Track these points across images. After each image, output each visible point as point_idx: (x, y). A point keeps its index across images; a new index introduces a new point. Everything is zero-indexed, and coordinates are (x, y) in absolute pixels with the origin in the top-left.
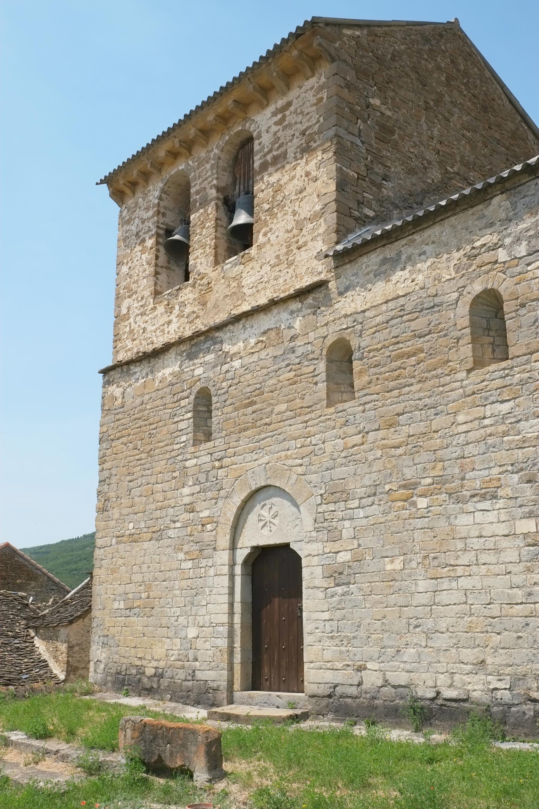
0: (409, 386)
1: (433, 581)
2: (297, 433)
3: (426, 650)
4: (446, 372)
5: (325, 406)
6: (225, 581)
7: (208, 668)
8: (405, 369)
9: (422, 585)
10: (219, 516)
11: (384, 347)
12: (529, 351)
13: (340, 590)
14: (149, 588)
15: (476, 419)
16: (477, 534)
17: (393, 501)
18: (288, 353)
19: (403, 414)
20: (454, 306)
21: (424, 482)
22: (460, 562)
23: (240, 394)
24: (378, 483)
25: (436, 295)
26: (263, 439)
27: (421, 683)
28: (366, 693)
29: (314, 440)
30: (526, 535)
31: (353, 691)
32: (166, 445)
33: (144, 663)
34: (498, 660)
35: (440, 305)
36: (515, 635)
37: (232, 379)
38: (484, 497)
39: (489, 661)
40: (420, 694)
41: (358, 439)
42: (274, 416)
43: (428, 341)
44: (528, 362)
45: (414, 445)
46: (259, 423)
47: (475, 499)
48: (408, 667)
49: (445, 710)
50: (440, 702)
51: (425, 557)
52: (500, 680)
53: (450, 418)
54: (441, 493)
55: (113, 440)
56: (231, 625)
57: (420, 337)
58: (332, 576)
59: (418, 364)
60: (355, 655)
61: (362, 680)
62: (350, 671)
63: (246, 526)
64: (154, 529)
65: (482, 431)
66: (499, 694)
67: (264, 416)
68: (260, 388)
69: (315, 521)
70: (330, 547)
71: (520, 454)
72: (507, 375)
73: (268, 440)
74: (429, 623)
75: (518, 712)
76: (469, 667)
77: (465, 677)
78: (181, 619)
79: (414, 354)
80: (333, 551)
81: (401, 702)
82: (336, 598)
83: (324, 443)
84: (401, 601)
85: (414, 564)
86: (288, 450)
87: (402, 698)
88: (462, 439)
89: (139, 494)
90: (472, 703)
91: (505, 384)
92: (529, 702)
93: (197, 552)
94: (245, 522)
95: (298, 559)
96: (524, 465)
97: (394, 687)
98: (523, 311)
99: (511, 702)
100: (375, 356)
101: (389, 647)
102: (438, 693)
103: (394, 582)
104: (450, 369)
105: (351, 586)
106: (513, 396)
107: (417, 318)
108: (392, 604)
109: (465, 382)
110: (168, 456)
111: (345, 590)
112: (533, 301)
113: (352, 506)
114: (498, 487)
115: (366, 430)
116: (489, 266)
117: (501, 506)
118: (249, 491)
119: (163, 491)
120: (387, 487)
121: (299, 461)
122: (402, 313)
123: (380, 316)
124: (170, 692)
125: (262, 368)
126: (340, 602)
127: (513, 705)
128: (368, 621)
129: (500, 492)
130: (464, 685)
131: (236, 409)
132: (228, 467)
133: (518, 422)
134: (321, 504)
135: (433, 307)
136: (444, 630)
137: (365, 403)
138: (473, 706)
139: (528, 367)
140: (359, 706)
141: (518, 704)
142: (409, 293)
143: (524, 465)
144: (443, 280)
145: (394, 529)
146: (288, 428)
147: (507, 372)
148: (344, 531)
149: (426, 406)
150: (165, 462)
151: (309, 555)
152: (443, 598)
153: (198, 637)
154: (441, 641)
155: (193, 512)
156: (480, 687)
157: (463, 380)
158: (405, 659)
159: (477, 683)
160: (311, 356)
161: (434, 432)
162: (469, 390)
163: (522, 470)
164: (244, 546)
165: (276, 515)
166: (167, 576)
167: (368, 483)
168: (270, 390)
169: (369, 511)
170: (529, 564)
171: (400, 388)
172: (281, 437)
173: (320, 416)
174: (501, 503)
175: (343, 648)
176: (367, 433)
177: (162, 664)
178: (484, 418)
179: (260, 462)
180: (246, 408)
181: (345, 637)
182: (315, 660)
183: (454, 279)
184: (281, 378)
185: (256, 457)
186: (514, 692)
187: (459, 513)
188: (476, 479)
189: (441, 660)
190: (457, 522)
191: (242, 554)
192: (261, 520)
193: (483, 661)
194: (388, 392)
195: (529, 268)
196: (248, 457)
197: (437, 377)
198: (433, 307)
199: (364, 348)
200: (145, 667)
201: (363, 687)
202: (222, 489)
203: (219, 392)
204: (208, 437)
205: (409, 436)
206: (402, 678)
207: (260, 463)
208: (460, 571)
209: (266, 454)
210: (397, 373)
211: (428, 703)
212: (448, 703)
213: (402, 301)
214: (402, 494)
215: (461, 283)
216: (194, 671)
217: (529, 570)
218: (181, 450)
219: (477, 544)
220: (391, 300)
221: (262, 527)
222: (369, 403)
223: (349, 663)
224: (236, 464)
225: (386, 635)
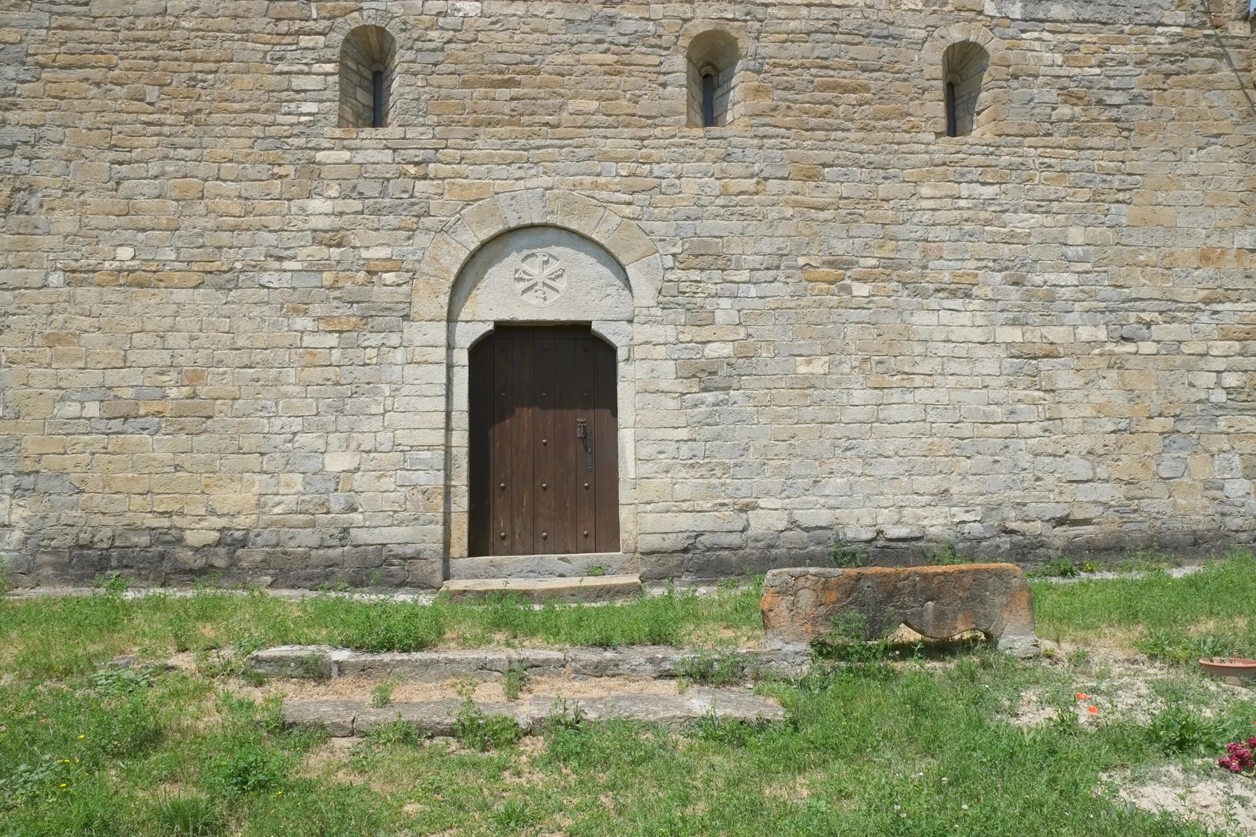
0: (843, 130)
1: (877, 391)
2: (621, 153)
3: (862, 479)
4: (904, 127)
5: (684, 122)
6: (440, 374)
7: (389, 521)
8: (837, 106)
9: (859, 396)
10: (419, 261)
11: (802, 66)
12: (1022, 132)
13: (710, 397)
14: (195, 377)
15: (947, 196)
16: (943, 337)
17: (810, 281)
18: (599, 23)
19: (831, 166)
20: (919, 47)
21: (862, 261)
22: (918, 369)
23: (478, 60)
24: (785, 252)
25: (892, 23)
26: (538, 148)
27: (854, 522)
28: (757, 541)
29: (657, 170)
30: (1009, 345)
31: (735, 539)
32: (249, 111)
33: (178, 521)
34: (967, 488)
35: (900, 38)
36: (991, 459)
37: (455, 30)
38: (953, 294)
39: (955, 489)
40: (850, 535)
41: (749, 184)
42: (565, 114)
43: (877, 80)
44: (1020, 145)
45: (851, 212)
46: (525, 119)
47: (940, 295)
48: (832, 502)
50: (881, 543)
51: (865, 360)
52: (968, 512)
53: (910, 188)
54: (890, 281)
55: (43, 66)
56: (448, 447)
57: (864, 71)
58: (694, 376)
59: (861, 105)
60: (738, 489)
62: (726, 512)
63: (481, 285)
64: (208, 267)
65: (957, 213)
66: (966, 528)
67: (541, 110)
68: (533, 63)
69: (659, 292)
70: (689, 334)
71: (1005, 250)
72: (992, 154)
73: (550, 150)
74: (870, 445)
75: (991, 546)
76: (926, 498)
77: (920, 511)
78: (301, 439)
79: (854, 91)
80: (699, 339)
81: (819, 548)
82: (703, 409)
83: (679, 177)
84: (823, 415)
85: (846, 368)
86: (599, 175)
87: (818, 544)
88: (926, 217)
89: (157, 192)
90: (930, 541)
91: (989, 163)
93: (354, 319)
94: (480, 278)
95: (611, 350)
96: (1011, 264)
97: (807, 529)
98: (1014, 84)
100: (784, 75)
101: (800, 477)
103: (811, 391)
104: (911, 124)
105: (732, 392)
106: (999, 180)
107: (861, 43)
108: (808, 419)
109: (932, 147)
110: (255, 131)
111: (721, 397)
112: (1029, 76)
113: (735, 279)
114: (974, 285)
115: (763, 174)
116: (972, 14)
117: (976, 307)
118: (501, 227)
119: (239, 197)
120: (801, 261)
121: (627, 198)
122: (834, 29)
123: (797, 22)
124: (272, 572)
125: (535, 30)
126: (710, 415)
127: (985, 539)
128: (765, 442)
129: (975, 291)
131: (465, 84)
132: (444, 179)
133: (1004, 212)
134: (672, 268)
135: (886, 37)
136: (891, 453)
137: (765, 137)
139: (1020, 151)
140: (743, 560)
142: (848, 6)
143: (1011, 264)
144: (903, 7)
145: (812, 319)
146: (601, 141)
147: (991, 149)
148: (718, 313)
149: (870, 163)
150: (249, 142)
151: (647, 343)
152: (893, 413)
153: (358, 469)
154: (884, 468)
155: (339, 245)
156: (942, 521)
157: (929, 144)
158: (827, 492)
159: (937, 517)
160: (653, 41)
161: (882, 200)
162: (938, 157)
163: (1007, 269)
164: (476, 318)
165: (561, 276)
166: (258, 358)
167: (767, 250)
168: (558, 71)
169: (767, 289)
170: (1011, 378)
171: (827, 130)
172: (583, 152)
173: (673, 136)
174: (976, 304)
175: (713, 481)
176: (766, 179)
177: (243, 521)
178: (959, 198)
179: (531, 183)
180: (494, 87)
181: (718, 464)
182: (656, 499)
183: (920, 11)
184: (583, 58)
185: (520, 173)
187: (917, 309)
188: (944, 271)
189: (886, 491)
190: (913, 320)
191: (468, 334)
192: (521, 279)
193: (946, 491)
194: (807, 130)
195: (1024, 36)
196: (501, 171)
197: (891, 129)
198: (886, 37)
199: (764, 58)
200: (182, 530)
201: (749, 533)
202: (427, 214)
203: (419, 45)
204: (376, 117)
205: (841, 198)
206: (823, 517)
207: (529, 185)
208: (918, 380)
209: (545, 173)
210: (824, 108)
212: (893, 544)
213: (836, 13)
214: (828, 274)
215: (932, 20)
216: (345, 530)
217: (1011, 385)
218: (301, 128)
219: (944, 349)
220: (815, 5)
221: (524, 292)
222: (771, 137)
223: (726, 501)
224: (467, 177)
225: (797, 461)
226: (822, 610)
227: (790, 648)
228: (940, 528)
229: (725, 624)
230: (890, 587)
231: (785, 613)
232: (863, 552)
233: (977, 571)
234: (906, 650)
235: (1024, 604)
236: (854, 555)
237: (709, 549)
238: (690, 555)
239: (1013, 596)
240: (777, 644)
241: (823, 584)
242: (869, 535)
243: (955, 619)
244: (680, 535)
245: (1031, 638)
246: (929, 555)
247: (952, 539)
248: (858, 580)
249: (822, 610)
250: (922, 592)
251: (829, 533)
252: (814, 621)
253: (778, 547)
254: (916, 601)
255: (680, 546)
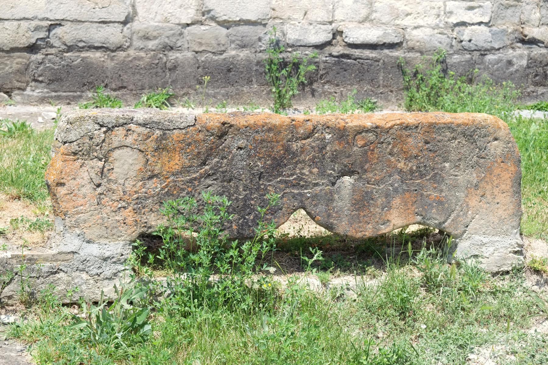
27: (299, 16)
28: (147, 38)
31: (113, 35)
40: (292, 36)
49: (348, 65)
52: (471, 8)
61: (135, 13)
66: (467, 33)
75: (499, 61)
81: (243, 54)
87: (243, 46)
92: (519, 45)
97: (226, 24)
99: (488, 46)
102: (337, 33)
127: (492, 50)
130: (397, 17)
138: (411, 55)
140: (124, 66)
141: (499, 49)
156: (432, 21)
186: (494, 28)
201: (136, 25)
211: (311, 53)
212: (357, 52)
226: (155, 186)
227: (94, 250)
228: (428, 31)
229: (14, 191)
230: (278, 149)
231: (88, 189)
232: (310, 63)
233: (432, 127)
234: (291, 254)
235: (507, 185)
236: (296, 66)
237: (70, 49)
238: (39, 57)
239: (489, 170)
240: (72, 243)
241: (160, 140)
242: (322, 37)
243: (387, 206)
244: (24, 25)
245: (514, 240)
246: (408, 70)
247: (444, 48)
248: (222, 135)
249: (155, 186)
250: (334, 158)
251: (259, 31)
252: (140, 204)
253: (179, 49)
254: (322, 174)
255: (24, 42)
